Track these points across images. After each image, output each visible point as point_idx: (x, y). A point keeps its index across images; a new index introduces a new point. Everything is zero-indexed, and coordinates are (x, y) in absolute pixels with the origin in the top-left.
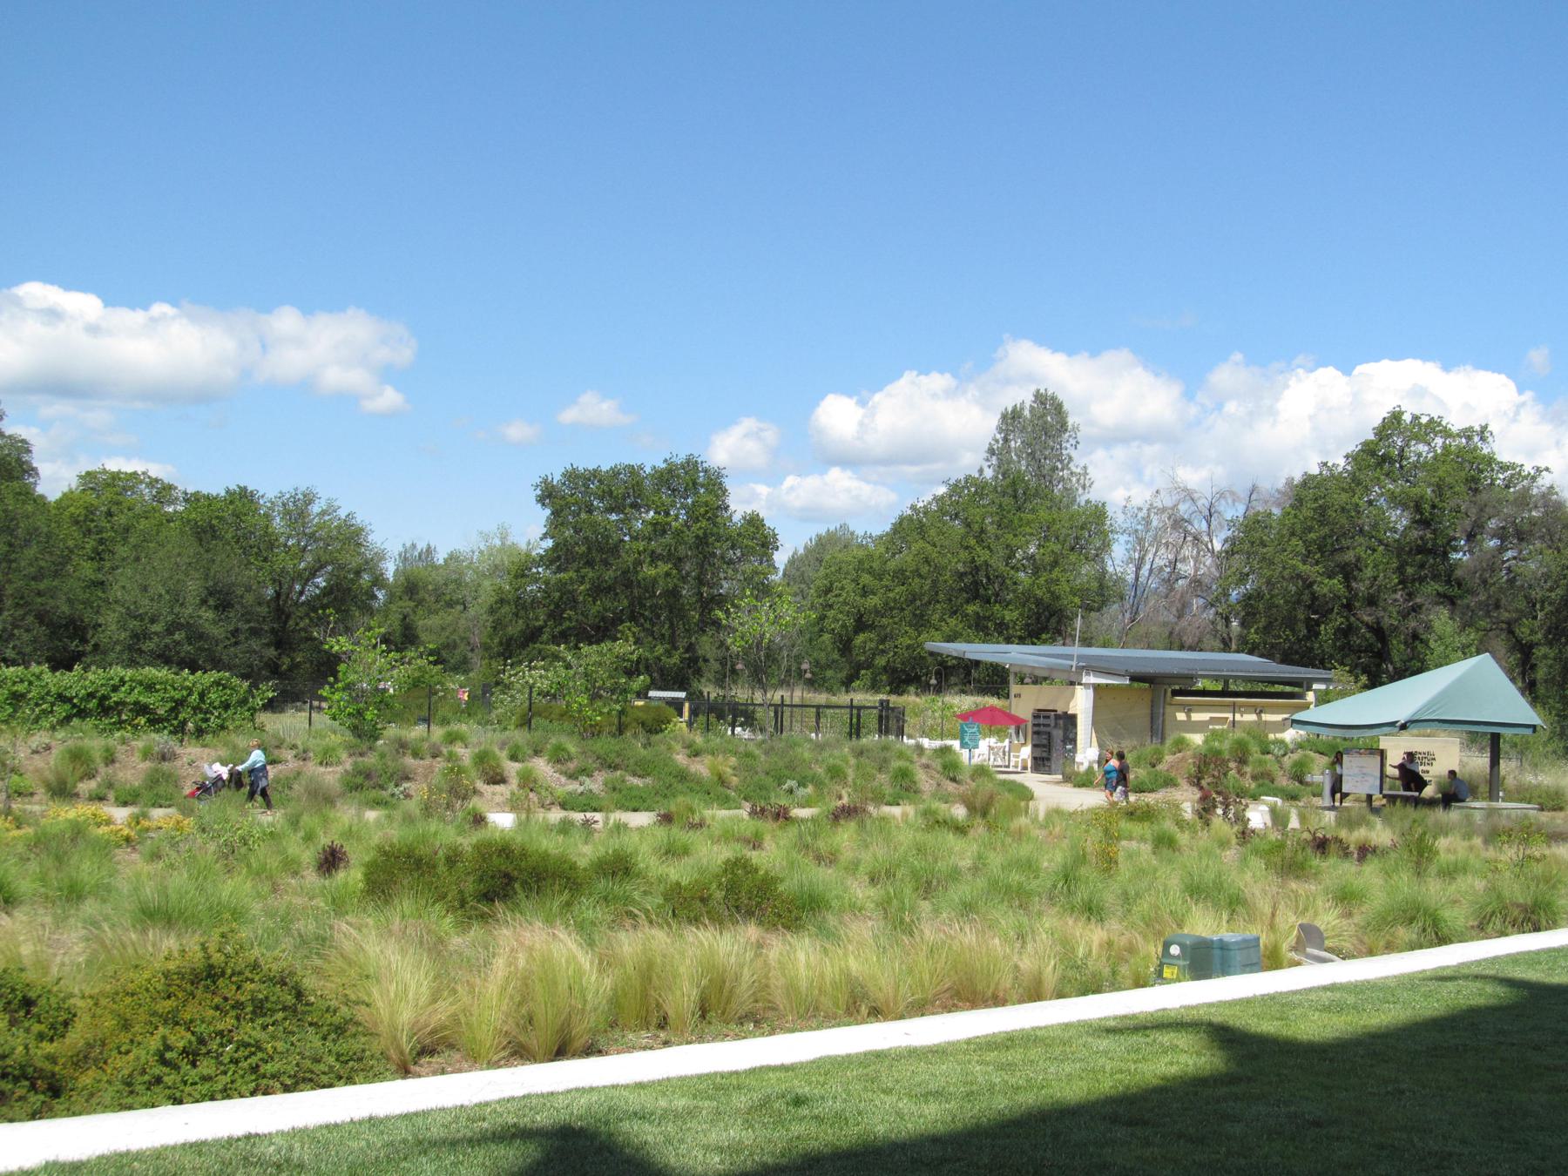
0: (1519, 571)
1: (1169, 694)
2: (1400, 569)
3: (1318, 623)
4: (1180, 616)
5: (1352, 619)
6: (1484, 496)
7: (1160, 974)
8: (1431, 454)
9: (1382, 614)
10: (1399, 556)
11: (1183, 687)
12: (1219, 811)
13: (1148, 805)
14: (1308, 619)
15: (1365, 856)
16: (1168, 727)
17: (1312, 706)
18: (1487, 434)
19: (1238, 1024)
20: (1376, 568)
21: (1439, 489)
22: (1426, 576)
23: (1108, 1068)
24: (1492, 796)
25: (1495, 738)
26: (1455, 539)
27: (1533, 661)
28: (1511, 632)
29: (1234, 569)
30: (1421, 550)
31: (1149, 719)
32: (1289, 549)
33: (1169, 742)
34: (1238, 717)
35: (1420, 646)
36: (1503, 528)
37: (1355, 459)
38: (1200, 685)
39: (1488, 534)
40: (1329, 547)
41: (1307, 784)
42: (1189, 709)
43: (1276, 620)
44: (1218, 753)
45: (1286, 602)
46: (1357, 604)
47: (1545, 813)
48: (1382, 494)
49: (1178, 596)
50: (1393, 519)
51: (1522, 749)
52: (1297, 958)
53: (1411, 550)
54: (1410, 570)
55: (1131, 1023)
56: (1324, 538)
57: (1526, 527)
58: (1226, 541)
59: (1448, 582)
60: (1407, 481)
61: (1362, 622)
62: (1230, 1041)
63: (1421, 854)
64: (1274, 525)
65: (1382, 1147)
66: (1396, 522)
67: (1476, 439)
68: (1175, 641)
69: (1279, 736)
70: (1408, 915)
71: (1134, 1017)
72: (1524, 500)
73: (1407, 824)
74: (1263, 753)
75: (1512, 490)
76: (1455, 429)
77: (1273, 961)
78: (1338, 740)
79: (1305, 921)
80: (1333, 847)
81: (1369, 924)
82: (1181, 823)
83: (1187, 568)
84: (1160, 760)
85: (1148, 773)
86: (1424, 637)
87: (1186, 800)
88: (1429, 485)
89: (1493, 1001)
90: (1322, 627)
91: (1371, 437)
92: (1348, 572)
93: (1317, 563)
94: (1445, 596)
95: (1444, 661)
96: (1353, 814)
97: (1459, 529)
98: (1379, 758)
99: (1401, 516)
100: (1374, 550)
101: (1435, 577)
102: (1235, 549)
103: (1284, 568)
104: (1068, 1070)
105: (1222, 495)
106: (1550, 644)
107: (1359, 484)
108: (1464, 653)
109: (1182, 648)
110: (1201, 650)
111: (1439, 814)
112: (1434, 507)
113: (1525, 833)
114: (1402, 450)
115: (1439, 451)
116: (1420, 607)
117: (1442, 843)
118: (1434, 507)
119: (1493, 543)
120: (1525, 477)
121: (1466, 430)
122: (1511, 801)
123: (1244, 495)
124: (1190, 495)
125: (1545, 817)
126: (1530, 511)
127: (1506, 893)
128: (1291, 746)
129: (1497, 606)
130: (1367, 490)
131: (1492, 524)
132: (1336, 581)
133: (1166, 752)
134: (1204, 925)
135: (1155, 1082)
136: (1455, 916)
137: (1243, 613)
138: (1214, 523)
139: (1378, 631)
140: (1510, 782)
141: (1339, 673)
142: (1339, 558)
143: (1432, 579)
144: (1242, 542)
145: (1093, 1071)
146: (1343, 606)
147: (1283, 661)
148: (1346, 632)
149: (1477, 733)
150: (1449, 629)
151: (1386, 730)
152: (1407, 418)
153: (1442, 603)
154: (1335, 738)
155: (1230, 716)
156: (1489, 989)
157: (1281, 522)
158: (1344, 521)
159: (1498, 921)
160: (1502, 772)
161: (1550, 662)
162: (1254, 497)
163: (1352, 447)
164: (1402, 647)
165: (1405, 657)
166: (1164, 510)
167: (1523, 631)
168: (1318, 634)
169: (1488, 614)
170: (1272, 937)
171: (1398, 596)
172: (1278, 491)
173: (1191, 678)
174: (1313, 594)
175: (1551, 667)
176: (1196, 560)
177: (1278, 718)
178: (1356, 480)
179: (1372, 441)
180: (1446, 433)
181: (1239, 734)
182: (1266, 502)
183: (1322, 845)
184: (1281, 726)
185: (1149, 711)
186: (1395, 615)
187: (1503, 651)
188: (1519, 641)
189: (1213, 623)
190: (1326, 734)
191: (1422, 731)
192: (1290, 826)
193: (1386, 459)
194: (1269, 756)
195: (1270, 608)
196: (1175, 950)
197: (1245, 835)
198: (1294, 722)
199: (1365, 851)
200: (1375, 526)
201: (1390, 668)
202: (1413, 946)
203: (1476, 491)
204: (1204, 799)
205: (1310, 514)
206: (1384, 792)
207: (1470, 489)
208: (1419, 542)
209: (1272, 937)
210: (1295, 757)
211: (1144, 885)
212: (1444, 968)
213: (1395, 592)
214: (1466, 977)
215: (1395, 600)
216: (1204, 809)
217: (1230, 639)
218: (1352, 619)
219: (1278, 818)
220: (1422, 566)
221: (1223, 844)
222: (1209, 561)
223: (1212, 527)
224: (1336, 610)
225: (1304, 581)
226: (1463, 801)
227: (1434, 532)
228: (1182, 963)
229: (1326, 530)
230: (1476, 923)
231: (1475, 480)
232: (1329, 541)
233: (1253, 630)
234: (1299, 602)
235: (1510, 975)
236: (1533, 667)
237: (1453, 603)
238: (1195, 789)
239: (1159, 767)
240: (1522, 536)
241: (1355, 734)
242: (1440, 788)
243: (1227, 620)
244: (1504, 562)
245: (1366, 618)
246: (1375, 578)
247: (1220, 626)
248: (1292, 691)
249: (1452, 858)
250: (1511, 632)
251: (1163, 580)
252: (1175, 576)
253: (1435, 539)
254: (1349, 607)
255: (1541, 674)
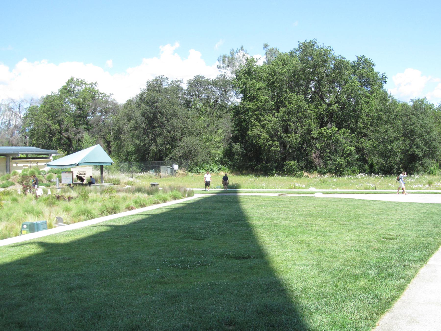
0: (106, 122)
1: (11, 159)
2: (74, 122)
3: (52, 137)
4: (11, 137)
5: (61, 136)
6: (96, 101)
7: (21, 232)
8: (82, 90)
9: (70, 134)
10: (74, 118)
11: (15, 157)
12: (29, 191)
13: (8, 191)
14: (49, 136)
15: (70, 200)
16: (11, 168)
17: (52, 161)
18: (97, 84)
19: (45, 241)
20: (68, 122)
21: (84, 99)
22: (81, 123)
23: (15, 254)
24: (102, 182)
25: (102, 167)
26: (89, 113)
27: (110, 146)
28: (104, 138)
29: (27, 122)
30: (80, 116)
31: (5, 167)
32: (43, 116)
33: (12, 173)
34: (31, 165)
35: (80, 143)
36: (101, 110)
37: (61, 91)
38: (20, 156)
39: (97, 111)
40: (54, 116)
41: (52, 182)
42: (17, 163)
43: (40, 136)
44: (26, 175)
45: (43, 131)
46: (63, 132)
47: (115, 186)
48: (69, 101)
49: (11, 130)
50: (72, 108)
51: (109, 170)
52: (56, 226)
53: (77, 116)
54: (77, 122)
55: (18, 244)
56: (53, 113)
57: (108, 110)
58: (24, 114)
59: (87, 125)
60: (76, 97)
61: (64, 137)
62: (44, 245)
63: (85, 197)
64: (38, 109)
65: (85, 262)
66: (73, 109)
67: (94, 86)
68: (10, 144)
69: (43, 169)
70: (83, 213)
71: (18, 243)
72: (107, 102)
73: (80, 191)
74: (39, 174)
75: (104, 100)
76: (88, 83)
77: (50, 227)
78: (60, 170)
79: (58, 216)
80: (61, 198)
81: (74, 216)
82: (18, 195)
83: (13, 122)
84: (9, 178)
85: (6, 182)
86: (81, 140)
87: (19, 188)
88: (82, 98)
89: (106, 230)
90: (53, 138)
91: (65, 85)
92: (60, 123)
93: (51, 120)
94: (87, 129)
95: (87, 147)
96: (66, 189)
97: (90, 110)
98: (71, 174)
99: (74, 107)
100: (67, 116)
101: (84, 124)
102: (27, 117)
103: (42, 122)
104: (5, 256)
105: (23, 101)
106: (115, 141)
107: (62, 98)
108: (92, 144)
109: (12, 145)
110: (18, 146)
111: (88, 188)
112: (83, 104)
113: (111, 191)
114: (74, 88)
115: (84, 89)
116: (80, 132)
117: (90, 195)
118: (83, 104)
119: (99, 114)
120: (107, 96)
121: (91, 83)
122: (106, 183)
123: (29, 101)
124: (13, 101)
125: (115, 186)
126: (108, 105)
127: (107, 206)
128: (47, 172)
129: (101, 131)
130: (64, 100)
131: (99, 109)
132: (56, 125)
133: (11, 176)
134: (31, 219)
135: (28, 256)
136: (96, 212)
137: (30, 135)
138: (21, 109)
139: (69, 139)
140: (106, 178)
141: (60, 151)
142: (57, 119)
143: (83, 124)
144: (29, 114)
145: (11, 255)
146: (59, 132)
147: (42, 148)
148: (60, 139)
149: (96, 165)
150: (88, 138)
151: (73, 166)
152: (75, 80)
153: (86, 131)
154: (59, 169)
155: (29, 164)
156: (105, 228)
157: (40, 108)
158: (58, 108)
159: (105, 212)
160: (104, 176)
161: (115, 146)
162: (32, 101)
163: (60, 87)
164: (75, 143)
165: (76, 146)
166: (5, 105)
167: (108, 138)
168: (52, 140)
169: (98, 133)
170: (49, 221)
171: (74, 129)
172: (39, 100)
173: (17, 154)
174: (50, 129)
175: (115, 147)
176: (16, 120)
177: (43, 164)
178: (61, 97)
179: (66, 86)
180: (86, 84)
181: (32, 169)
182: (36, 103)
183: (58, 198)
184: (44, 167)
185: (5, 164)
186: (73, 134)
187: (102, 143)
188: (106, 140)
189: (21, 138)
190: (57, 168)
191: (82, 166)
192: (48, 194)
193: (69, 91)
194: (41, 175)
195: (38, 133)
196: (25, 226)
197: (37, 197)
198: (48, 165)
199: (70, 199)
200: (67, 110)
201: (72, 149)
202: (85, 220)
203: (94, 100)
204: (24, 188)
205: (49, 106)
206: (73, 183)
207: (93, 99)
208: (79, 114)
209: (49, 221)
210: (48, 175)
211: (12, 211)
212: (93, 224)
213: (73, 128)
214: (99, 226)
215: (73, 130)
216: (24, 191)
217: (27, 142)
218: (61, 136)
219: (45, 192)
220: (80, 121)
221: (31, 200)
222: (19, 120)
223: (20, 110)
224: (57, 133)
225: (48, 125)
226: (94, 184)
227: (83, 111)
228: (27, 229)
229: (53, 111)
230: (100, 213)
231: (94, 97)
232: (54, 114)
233: (33, 140)
234: (46, 131)
235: (110, 224)
236: (110, 147)
237: (89, 131)
238: (21, 185)
239: (9, 180)
240: (106, 112)
241: (64, 167)
242: (88, 181)
243: (25, 137)
244: (102, 119)
245: (65, 135)
246: (67, 124)
247: (23, 138)
248: (46, 157)
249: (92, 198)
250: (104, 138)
251: (6, 126)
252: (9, 124)
253: (83, 113)
254: (60, 132)
255: (112, 149)
